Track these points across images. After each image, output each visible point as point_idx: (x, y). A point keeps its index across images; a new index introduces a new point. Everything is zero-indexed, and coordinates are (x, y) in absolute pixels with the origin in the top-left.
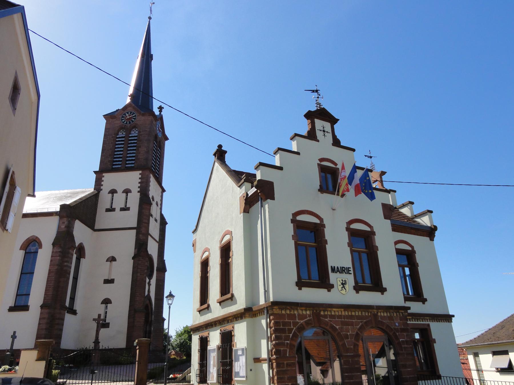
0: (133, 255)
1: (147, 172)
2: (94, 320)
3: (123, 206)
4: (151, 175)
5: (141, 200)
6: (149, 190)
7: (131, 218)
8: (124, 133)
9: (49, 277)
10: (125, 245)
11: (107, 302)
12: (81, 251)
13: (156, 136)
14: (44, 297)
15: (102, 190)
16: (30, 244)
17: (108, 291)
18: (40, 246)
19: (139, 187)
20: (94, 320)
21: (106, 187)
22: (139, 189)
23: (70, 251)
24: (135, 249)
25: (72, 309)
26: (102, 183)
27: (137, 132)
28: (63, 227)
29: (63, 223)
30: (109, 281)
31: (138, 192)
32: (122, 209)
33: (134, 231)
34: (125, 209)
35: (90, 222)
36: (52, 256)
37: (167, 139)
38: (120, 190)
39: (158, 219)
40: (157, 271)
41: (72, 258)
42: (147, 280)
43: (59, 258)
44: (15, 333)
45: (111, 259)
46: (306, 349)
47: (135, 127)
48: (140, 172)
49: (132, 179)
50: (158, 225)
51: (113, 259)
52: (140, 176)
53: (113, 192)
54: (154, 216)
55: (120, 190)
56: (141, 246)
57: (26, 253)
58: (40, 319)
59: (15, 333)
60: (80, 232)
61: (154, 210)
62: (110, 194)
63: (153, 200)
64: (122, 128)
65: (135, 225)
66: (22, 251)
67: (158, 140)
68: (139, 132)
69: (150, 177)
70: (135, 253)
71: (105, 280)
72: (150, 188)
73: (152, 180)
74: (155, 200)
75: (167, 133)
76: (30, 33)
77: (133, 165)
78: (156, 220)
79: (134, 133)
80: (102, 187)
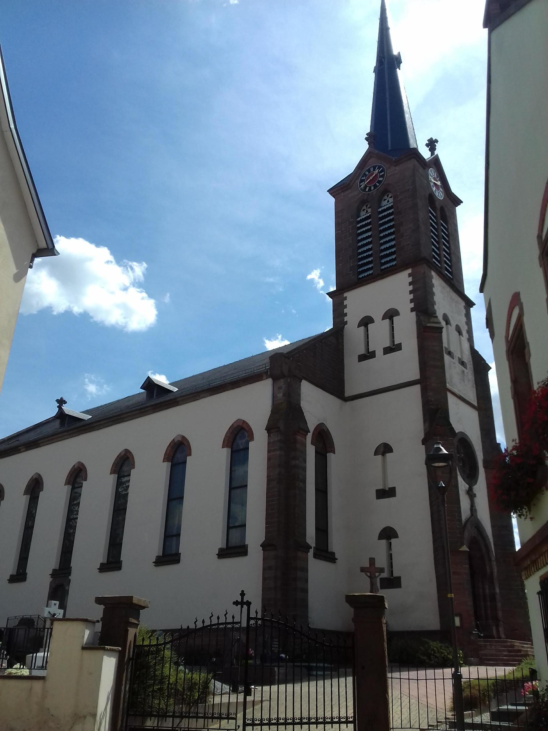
0: (422, 436)
1: (423, 268)
2: (363, 570)
3: (388, 344)
4: (433, 273)
5: (419, 323)
6: (434, 303)
7: (407, 364)
8: (369, 210)
9: (268, 489)
10: (403, 418)
11: (388, 534)
12: (324, 440)
13: (431, 198)
14: (266, 528)
15: (346, 323)
16: (236, 435)
17: (386, 513)
18: (251, 437)
19: (411, 301)
20: (363, 570)
21: (353, 318)
22: (412, 305)
23: (299, 438)
24: (425, 422)
25: (326, 551)
26: (345, 311)
27: (391, 200)
28: (280, 395)
29: (280, 388)
30: (385, 493)
31: (412, 310)
32: (388, 351)
33: (418, 388)
34: (393, 348)
35: (334, 384)
36: (269, 451)
37: (457, 202)
38: (377, 316)
39: (467, 357)
40: (485, 467)
41: (304, 453)
42: (462, 485)
43: (278, 452)
44: (243, 591)
45: (382, 450)
46: (84, 412)
47: (385, 192)
48: (410, 271)
49: (397, 289)
50: (469, 372)
51: (385, 449)
52: (410, 279)
53: (366, 322)
54: (457, 354)
55: (377, 316)
56: (435, 417)
57: (232, 452)
58: (264, 569)
59: (243, 591)
60: (315, 403)
61: (449, 338)
62: (362, 328)
63: (448, 322)
64: (364, 202)
65: (415, 375)
66: (225, 449)
67: (438, 207)
68: (395, 197)
69: (432, 277)
70: (425, 430)
71: (378, 491)
72: (436, 298)
73: (438, 286)
74: (454, 323)
75: (455, 189)
76: (472, 397)
77: (394, 263)
78: (463, 363)
79: (387, 202)
80: (346, 319)
